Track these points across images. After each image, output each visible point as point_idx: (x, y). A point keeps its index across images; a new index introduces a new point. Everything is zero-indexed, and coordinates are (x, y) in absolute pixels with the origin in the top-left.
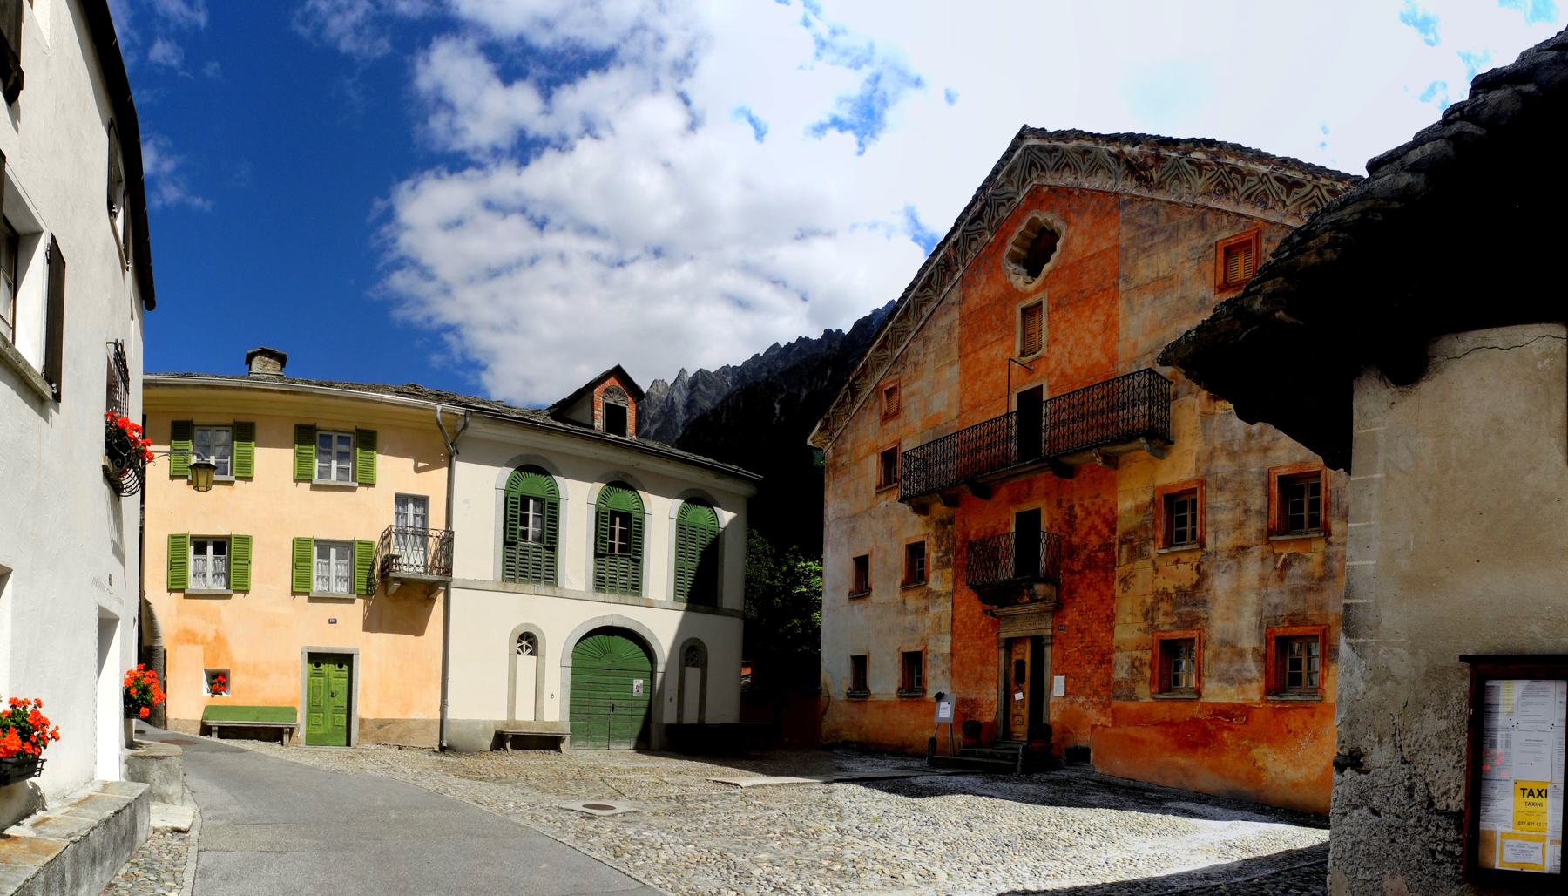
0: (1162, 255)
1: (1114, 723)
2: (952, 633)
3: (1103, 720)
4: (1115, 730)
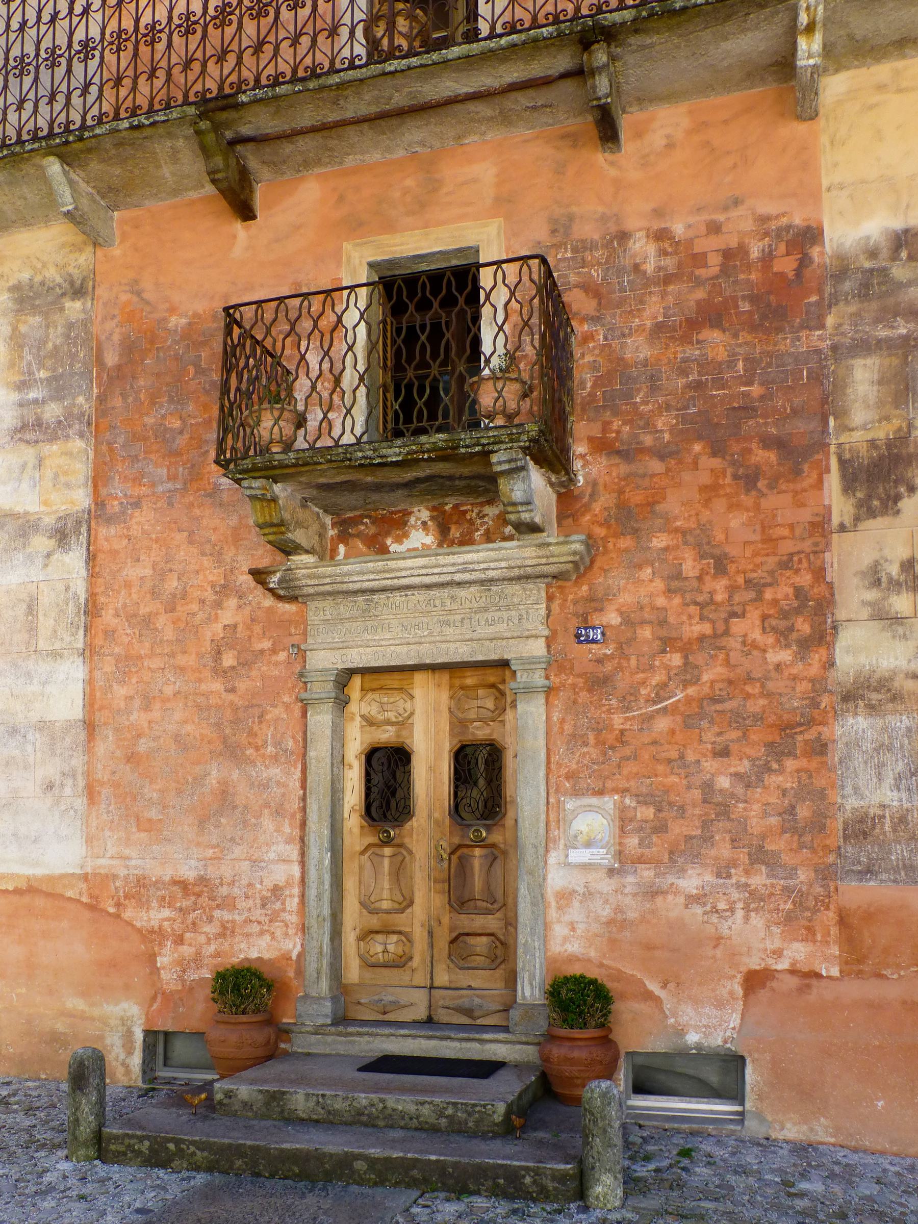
0: (604, 457)
1: (856, 960)
2: (90, 653)
3: (798, 952)
4: (854, 989)
